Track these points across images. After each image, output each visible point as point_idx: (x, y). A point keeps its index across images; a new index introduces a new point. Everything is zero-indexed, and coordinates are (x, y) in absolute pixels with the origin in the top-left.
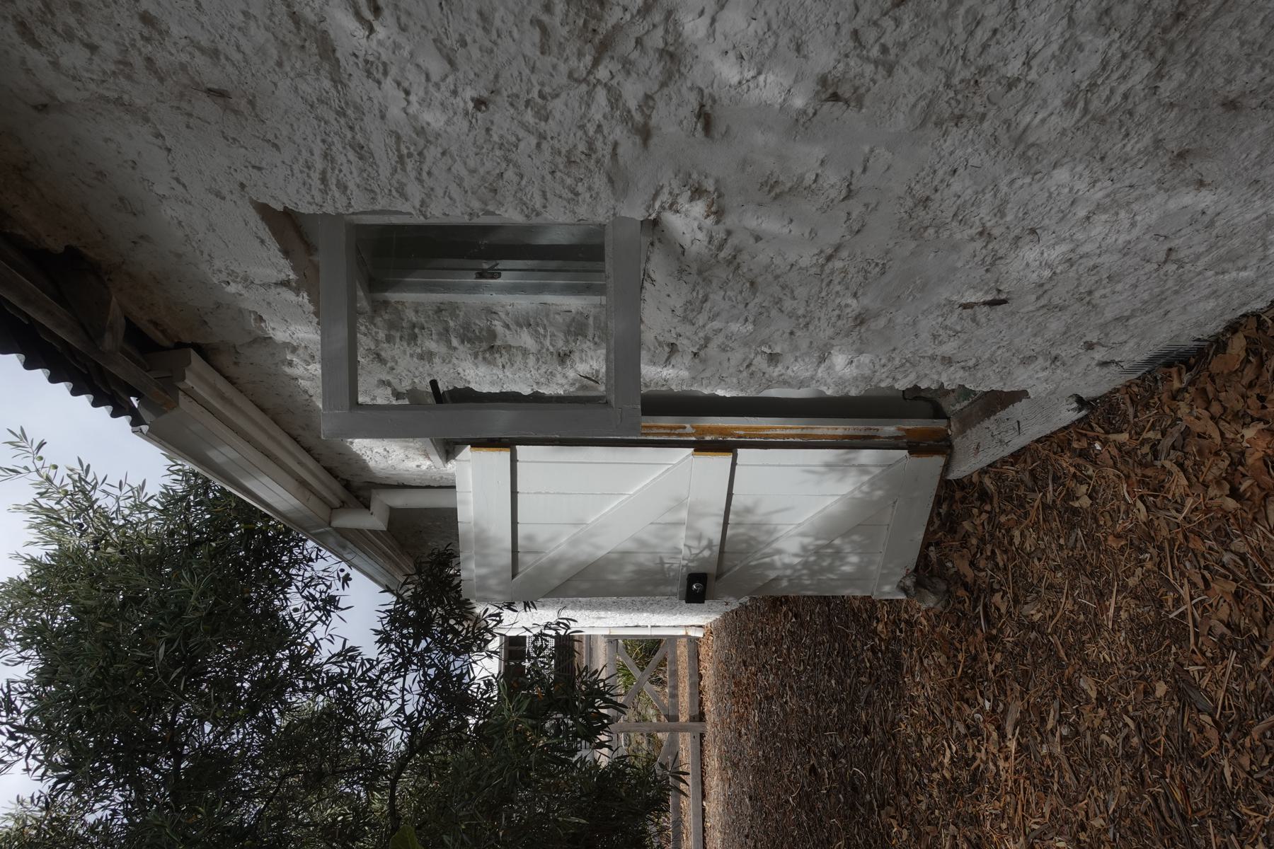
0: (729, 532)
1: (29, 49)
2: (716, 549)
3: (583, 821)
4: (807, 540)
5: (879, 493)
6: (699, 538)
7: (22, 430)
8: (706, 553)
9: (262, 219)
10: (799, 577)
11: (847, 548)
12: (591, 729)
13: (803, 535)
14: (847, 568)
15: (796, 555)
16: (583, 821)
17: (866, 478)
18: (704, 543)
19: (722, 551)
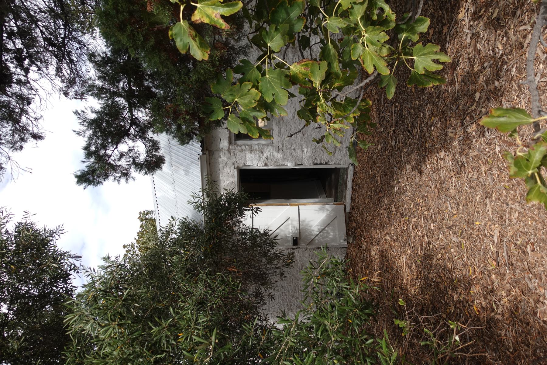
0: (301, 227)
1: (192, 40)
2: (298, 231)
3: (149, 323)
4: (319, 227)
5: (332, 214)
6: (294, 227)
7: (25, 212)
8: (296, 231)
9: (225, 21)
10: (320, 239)
11: (329, 231)
12: (241, 216)
13: (318, 226)
14: (331, 236)
15: (317, 231)
16: (149, 323)
17: (329, 212)
18: (295, 229)
19: (300, 232)
